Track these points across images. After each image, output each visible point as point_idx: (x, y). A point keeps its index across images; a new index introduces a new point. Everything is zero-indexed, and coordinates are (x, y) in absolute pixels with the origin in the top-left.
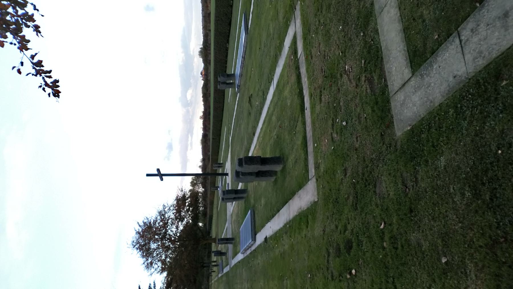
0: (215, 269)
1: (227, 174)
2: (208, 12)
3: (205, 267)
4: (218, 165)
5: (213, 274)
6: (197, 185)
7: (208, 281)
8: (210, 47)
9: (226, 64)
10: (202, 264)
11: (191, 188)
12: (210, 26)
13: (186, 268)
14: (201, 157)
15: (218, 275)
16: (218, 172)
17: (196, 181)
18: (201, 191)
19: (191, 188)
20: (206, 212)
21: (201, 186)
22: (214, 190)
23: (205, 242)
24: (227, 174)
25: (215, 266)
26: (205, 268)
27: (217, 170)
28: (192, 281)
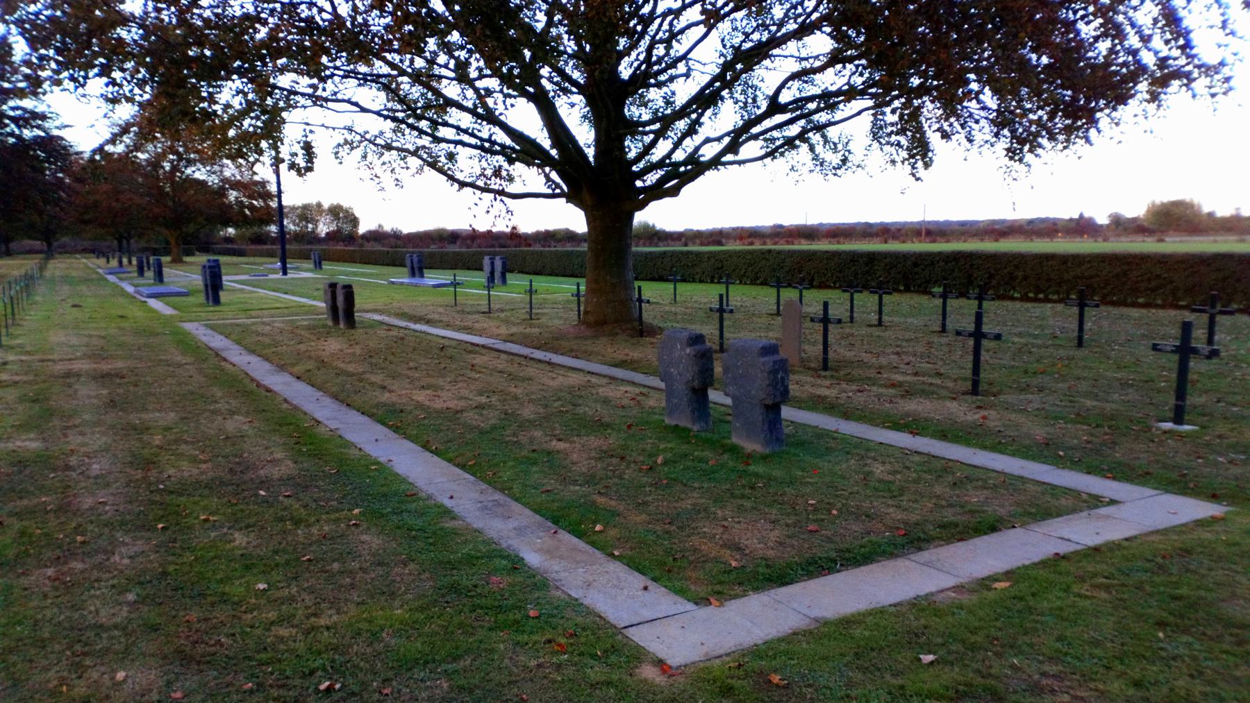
0: (114, 263)
1: (285, 273)
2: (724, 241)
3: (120, 242)
4: (416, 266)
5: (102, 261)
6: (333, 221)
7: (85, 251)
8: (650, 245)
9: (519, 272)
10: (125, 235)
11: (326, 205)
12: (694, 244)
13: (114, 204)
14: (406, 229)
15: (99, 267)
16: (288, 260)
17: (345, 217)
18: (319, 230)
19: (326, 205)
20: (265, 243)
21: (331, 229)
22: (408, 263)
23: (172, 241)
24: (285, 273)
25: (120, 262)
26: (116, 242)
27: (481, 269)
28: (86, 217)
